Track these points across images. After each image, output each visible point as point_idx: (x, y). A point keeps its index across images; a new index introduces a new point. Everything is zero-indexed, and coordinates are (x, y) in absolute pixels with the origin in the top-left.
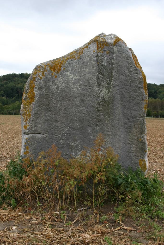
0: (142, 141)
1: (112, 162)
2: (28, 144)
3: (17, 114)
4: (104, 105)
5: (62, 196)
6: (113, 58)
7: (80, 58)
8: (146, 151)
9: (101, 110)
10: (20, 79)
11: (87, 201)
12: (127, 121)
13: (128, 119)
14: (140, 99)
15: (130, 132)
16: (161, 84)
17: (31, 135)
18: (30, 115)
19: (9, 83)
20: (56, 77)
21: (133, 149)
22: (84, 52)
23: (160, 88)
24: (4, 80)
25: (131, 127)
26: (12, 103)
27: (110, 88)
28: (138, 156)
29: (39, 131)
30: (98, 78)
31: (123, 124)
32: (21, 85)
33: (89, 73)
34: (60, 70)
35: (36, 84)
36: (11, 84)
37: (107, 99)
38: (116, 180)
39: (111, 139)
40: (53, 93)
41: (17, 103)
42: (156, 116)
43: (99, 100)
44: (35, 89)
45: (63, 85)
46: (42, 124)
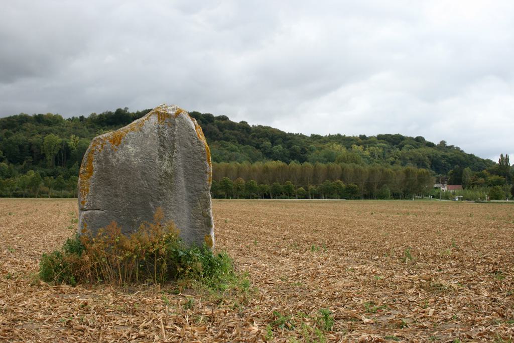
0: (207, 215)
1: (173, 236)
2: (86, 221)
3: (31, 197)
4: (166, 179)
5: (124, 274)
6: (175, 130)
7: (141, 131)
8: (212, 226)
9: (163, 184)
10: (36, 126)
11: (150, 278)
12: (191, 195)
13: (192, 192)
14: (204, 171)
15: (195, 206)
16: (313, 133)
17: (89, 211)
18: (88, 190)
19: (13, 133)
20: (116, 150)
21: (198, 224)
22: (145, 124)
23: (311, 142)
24: (4, 129)
25: (196, 201)
26: (20, 174)
27: (172, 160)
28: (204, 232)
29: (98, 207)
30: (159, 150)
31: (187, 198)
32: (39, 139)
33: (151, 145)
34: (119, 143)
35: (94, 157)
36: (20, 137)
37: (169, 172)
38: (176, 253)
39: (175, 213)
40: (113, 167)
41: (31, 174)
42: (302, 195)
43: (161, 173)
44: (93, 163)
45: (124, 158)
46: (102, 199)
